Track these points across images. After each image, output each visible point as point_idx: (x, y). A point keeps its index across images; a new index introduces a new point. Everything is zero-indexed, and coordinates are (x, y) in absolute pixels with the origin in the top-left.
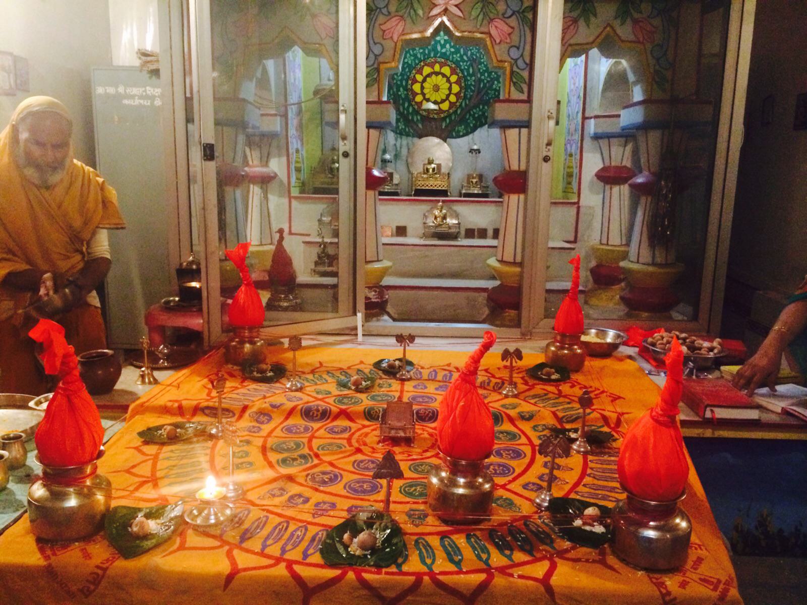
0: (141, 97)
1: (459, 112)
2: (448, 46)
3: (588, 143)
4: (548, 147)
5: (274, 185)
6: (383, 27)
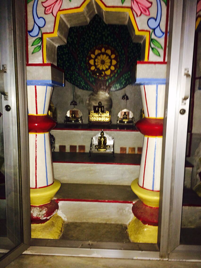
1: (116, 76)
2: (109, 38)
4: (184, 101)
6: (45, 5)
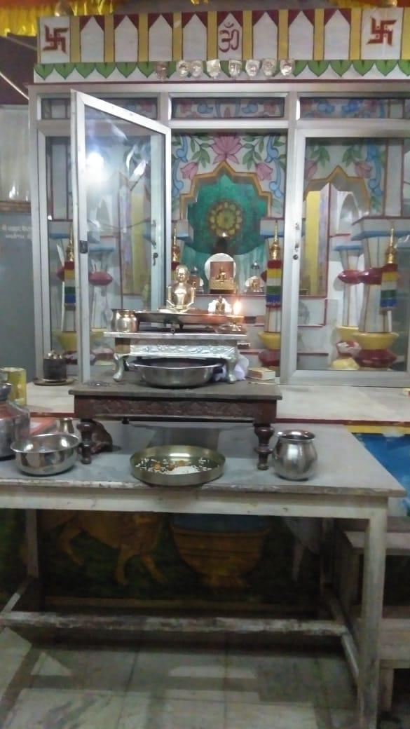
0: (18, 233)
3: (332, 254)
5: (110, 286)
